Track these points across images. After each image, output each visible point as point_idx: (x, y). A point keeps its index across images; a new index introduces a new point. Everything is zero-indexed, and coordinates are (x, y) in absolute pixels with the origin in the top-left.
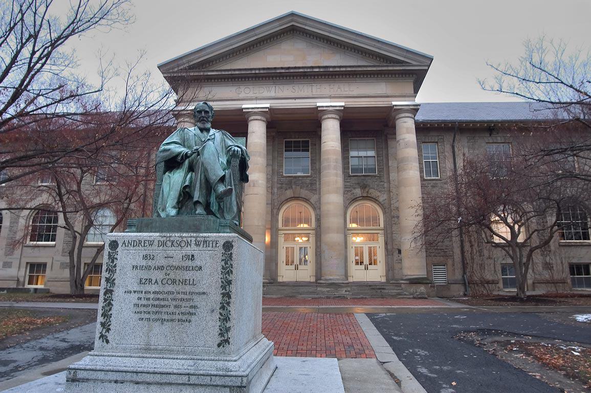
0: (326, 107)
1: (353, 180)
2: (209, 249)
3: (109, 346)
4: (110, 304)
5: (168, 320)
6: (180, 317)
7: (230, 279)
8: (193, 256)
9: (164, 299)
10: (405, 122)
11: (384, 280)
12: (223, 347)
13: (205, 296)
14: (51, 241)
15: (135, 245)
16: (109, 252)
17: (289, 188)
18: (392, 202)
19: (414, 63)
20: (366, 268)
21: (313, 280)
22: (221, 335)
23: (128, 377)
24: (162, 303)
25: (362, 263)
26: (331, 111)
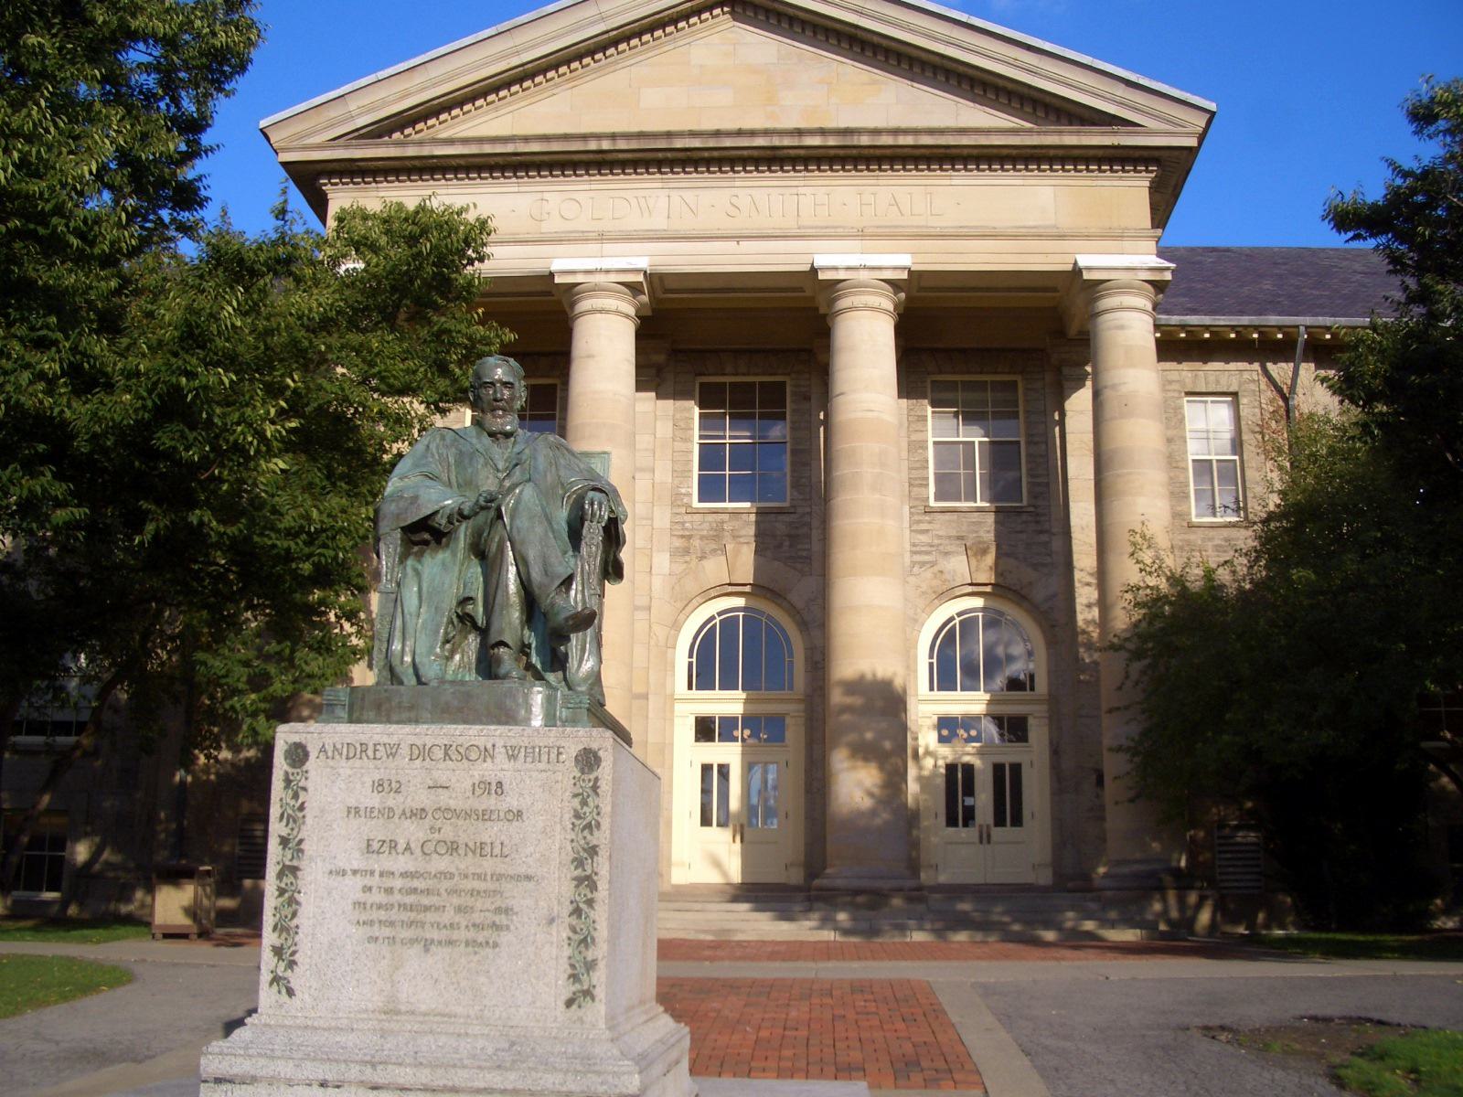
1: (942, 526)
2: (542, 766)
3: (296, 1001)
4: (292, 901)
5: (440, 942)
6: (471, 934)
7: (595, 842)
8: (500, 784)
9: (428, 892)
12: (580, 1007)
13: (531, 885)
14: (27, 734)
15: (414, 757)
16: (287, 773)
17: (714, 551)
21: (796, 877)
22: (574, 977)
23: (354, 1072)
24: (426, 901)
25: (969, 815)
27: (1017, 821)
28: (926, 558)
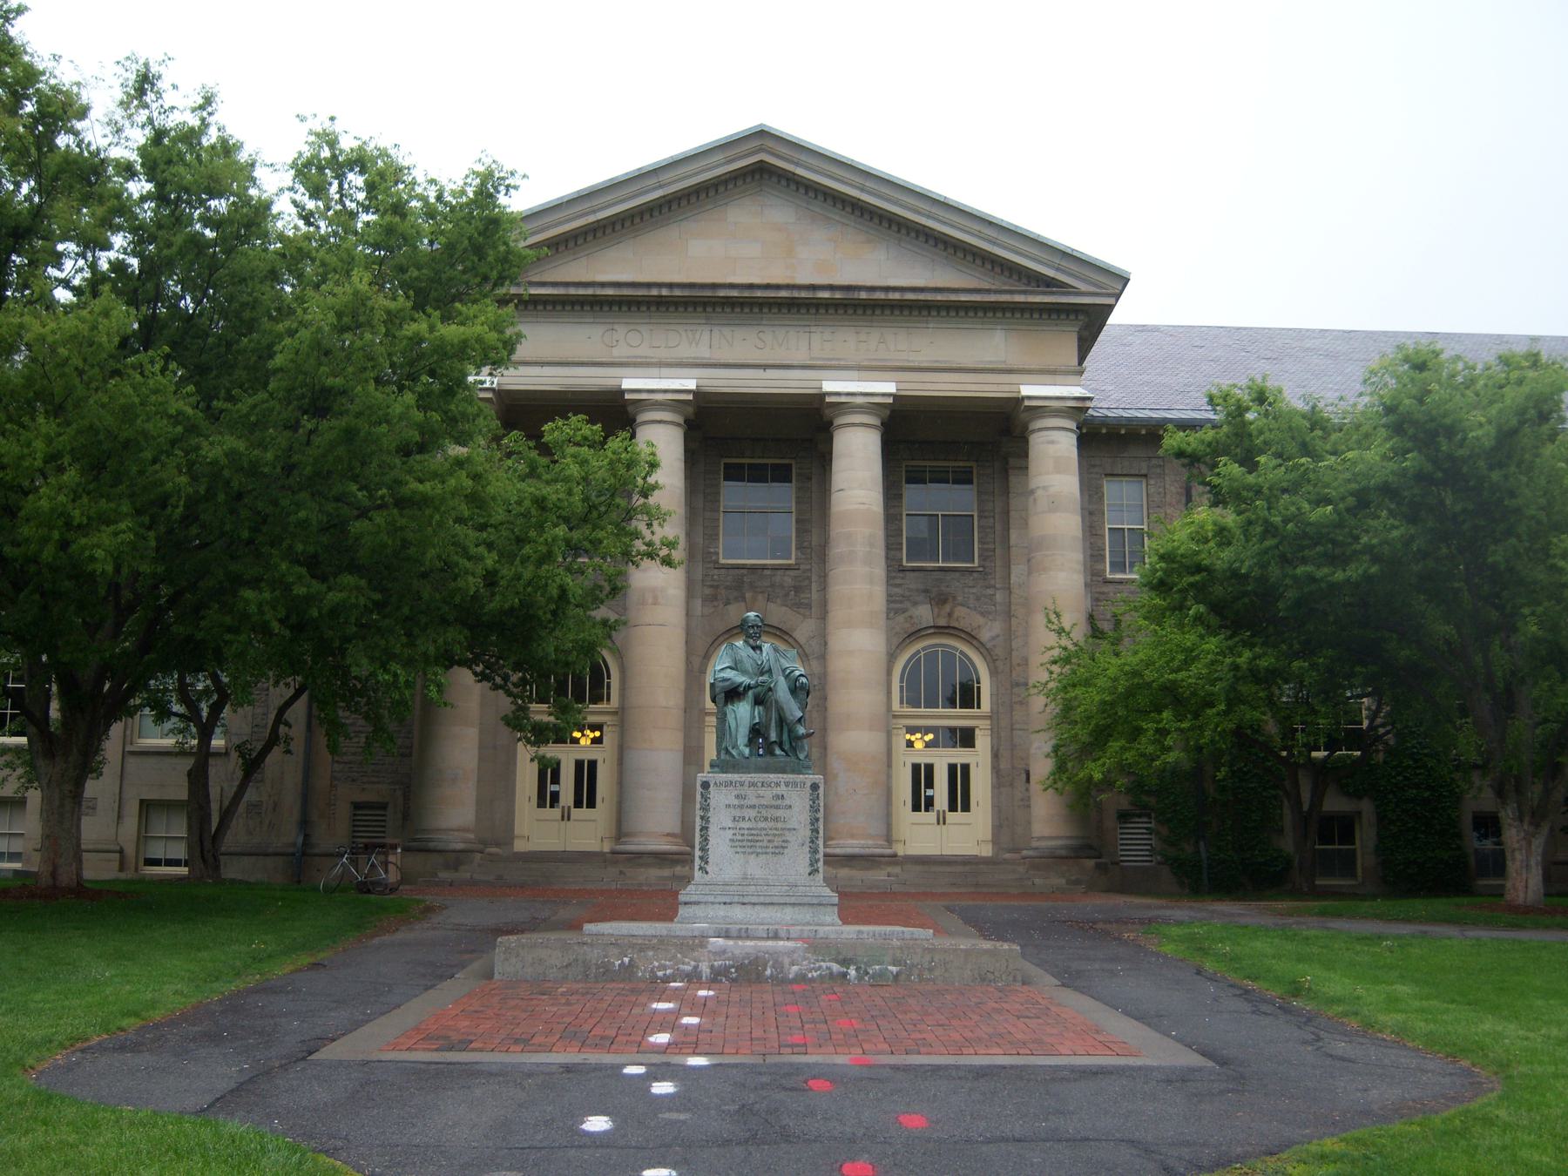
0: (848, 394)
4: (706, 839)
6: (773, 850)
10: (1052, 442)
11: (986, 851)
18: (1014, 645)
19: (1083, 287)
20: (941, 820)
22: (811, 865)
23: (736, 899)
25: (930, 802)
26: (860, 406)
27: (592, 804)
28: (899, 606)
